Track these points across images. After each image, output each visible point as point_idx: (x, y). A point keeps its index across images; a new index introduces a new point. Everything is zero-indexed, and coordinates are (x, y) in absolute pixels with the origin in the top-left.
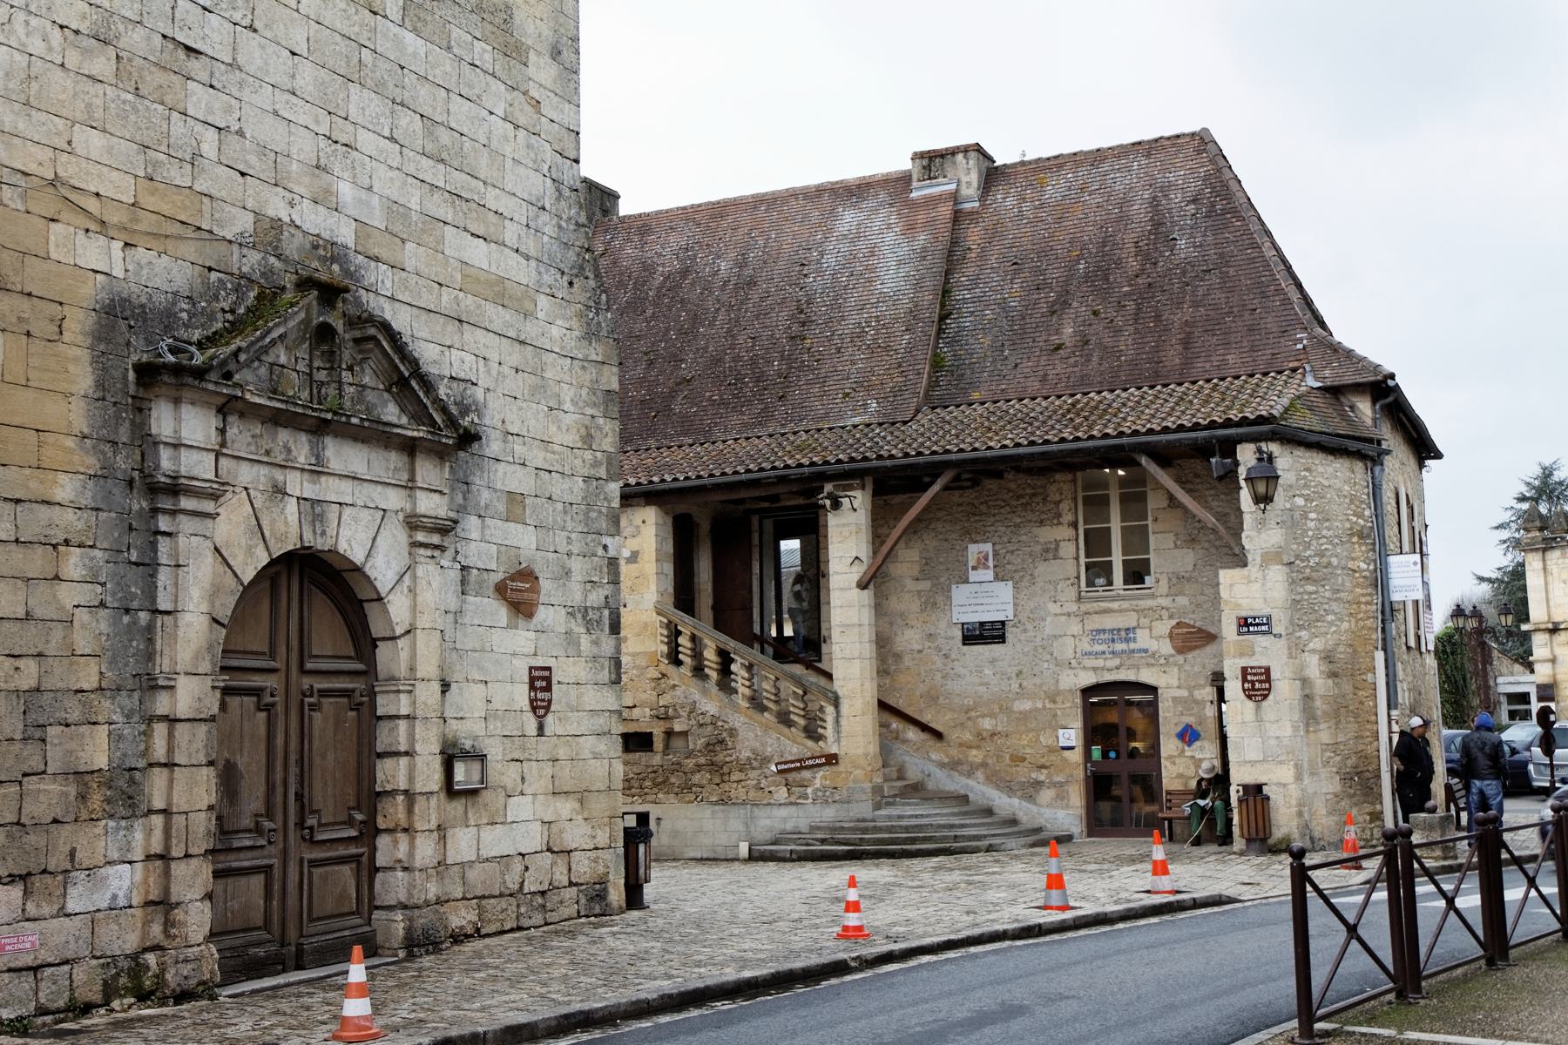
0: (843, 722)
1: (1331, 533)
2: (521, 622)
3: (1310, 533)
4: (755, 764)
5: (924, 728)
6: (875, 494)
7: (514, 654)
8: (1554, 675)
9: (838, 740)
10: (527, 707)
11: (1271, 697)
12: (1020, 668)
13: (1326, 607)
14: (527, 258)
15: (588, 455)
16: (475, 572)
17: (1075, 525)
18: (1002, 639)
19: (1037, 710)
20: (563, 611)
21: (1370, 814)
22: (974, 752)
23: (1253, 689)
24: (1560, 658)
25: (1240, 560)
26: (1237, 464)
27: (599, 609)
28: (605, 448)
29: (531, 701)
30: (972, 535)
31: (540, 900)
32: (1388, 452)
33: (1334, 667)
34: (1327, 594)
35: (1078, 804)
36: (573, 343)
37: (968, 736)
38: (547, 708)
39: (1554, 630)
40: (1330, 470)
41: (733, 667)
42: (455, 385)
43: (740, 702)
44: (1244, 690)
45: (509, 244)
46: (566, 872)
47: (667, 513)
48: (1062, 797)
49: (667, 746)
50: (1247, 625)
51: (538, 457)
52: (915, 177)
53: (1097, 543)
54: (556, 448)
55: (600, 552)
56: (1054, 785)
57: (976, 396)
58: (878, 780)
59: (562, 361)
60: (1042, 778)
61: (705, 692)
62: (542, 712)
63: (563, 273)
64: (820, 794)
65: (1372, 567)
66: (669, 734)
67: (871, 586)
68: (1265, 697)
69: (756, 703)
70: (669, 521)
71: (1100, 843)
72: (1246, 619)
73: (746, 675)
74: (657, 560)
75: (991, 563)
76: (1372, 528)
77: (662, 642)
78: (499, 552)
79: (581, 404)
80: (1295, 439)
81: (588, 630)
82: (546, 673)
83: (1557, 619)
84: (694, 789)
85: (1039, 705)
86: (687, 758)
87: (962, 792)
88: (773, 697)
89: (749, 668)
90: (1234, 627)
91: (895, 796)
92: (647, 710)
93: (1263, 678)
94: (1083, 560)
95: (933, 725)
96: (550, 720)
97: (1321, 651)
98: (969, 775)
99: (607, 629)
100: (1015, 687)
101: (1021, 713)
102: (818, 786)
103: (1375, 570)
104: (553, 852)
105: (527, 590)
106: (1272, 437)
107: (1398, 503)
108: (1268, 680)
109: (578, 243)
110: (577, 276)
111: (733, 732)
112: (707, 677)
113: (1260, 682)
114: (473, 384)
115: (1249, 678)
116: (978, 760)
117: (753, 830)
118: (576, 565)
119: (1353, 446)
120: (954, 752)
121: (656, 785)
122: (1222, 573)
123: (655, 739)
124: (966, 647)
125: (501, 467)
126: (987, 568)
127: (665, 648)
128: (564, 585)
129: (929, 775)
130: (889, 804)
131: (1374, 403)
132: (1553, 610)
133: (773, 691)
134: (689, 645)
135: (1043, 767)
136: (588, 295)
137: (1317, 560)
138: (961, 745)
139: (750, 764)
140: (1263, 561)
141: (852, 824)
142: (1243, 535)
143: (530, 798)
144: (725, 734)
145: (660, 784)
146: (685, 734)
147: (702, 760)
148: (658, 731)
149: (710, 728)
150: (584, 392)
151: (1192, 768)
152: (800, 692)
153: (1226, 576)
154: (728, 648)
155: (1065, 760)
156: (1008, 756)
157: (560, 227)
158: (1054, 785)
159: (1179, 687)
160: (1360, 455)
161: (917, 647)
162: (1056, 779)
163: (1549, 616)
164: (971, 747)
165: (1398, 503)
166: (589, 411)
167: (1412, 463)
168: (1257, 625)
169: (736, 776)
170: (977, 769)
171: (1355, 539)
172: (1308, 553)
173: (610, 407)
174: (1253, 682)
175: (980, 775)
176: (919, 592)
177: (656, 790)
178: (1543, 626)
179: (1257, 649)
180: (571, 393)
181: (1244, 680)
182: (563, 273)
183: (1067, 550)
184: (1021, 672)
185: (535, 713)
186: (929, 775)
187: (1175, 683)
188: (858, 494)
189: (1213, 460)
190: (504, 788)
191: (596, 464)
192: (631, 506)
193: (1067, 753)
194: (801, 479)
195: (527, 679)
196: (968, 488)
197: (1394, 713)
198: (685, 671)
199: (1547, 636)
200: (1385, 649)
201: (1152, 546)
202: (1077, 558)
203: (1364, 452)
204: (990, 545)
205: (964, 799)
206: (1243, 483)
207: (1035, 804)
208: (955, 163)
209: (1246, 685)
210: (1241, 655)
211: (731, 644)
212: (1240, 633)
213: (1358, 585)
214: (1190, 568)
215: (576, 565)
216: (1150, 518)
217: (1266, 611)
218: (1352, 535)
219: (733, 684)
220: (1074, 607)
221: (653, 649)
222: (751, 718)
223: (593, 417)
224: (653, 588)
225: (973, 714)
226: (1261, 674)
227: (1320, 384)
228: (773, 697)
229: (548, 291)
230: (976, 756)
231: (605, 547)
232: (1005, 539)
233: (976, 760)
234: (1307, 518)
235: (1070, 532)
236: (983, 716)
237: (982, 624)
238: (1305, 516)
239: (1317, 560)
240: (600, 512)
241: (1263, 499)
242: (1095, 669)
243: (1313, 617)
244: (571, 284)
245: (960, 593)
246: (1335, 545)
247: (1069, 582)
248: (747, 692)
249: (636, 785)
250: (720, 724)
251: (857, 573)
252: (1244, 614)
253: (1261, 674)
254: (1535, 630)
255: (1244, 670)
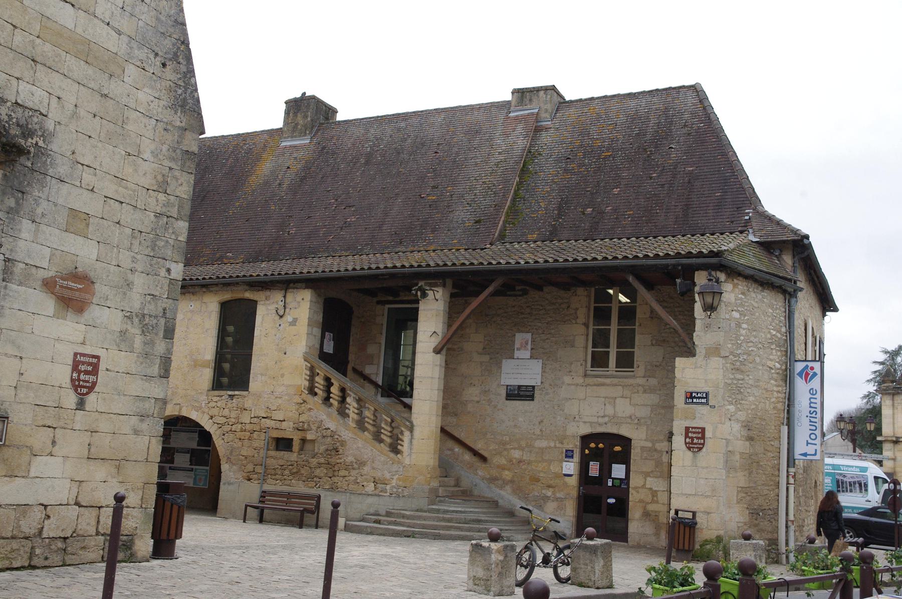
0: (415, 442)
1: (757, 340)
2: (70, 315)
3: (742, 338)
4: (356, 466)
5: (475, 453)
6: (452, 296)
7: (58, 340)
8: (894, 468)
9: (410, 455)
10: (69, 385)
11: (704, 450)
12: (542, 418)
13: (749, 390)
14: (119, 33)
15: (161, 197)
16: (22, 266)
17: (586, 325)
18: (531, 398)
19: (550, 447)
20: (121, 314)
21: (769, 540)
22: (507, 472)
23: (692, 443)
24: (899, 458)
25: (690, 352)
26: (694, 284)
27: (156, 317)
28: (179, 194)
29: (72, 380)
30: (521, 327)
31: (60, 544)
32: (801, 289)
33: (751, 433)
34: (751, 382)
35: (571, 514)
36: (160, 110)
37: (503, 461)
38: (91, 389)
39: (896, 442)
40: (760, 297)
41: (348, 400)
42: (20, 110)
43: (350, 423)
44: (686, 443)
45: (100, 17)
46: (94, 523)
47: (319, 295)
48: (561, 508)
49: (301, 449)
50: (692, 397)
51: (110, 188)
52: (513, 104)
53: (601, 339)
54: (129, 185)
55: (163, 272)
56: (557, 499)
57: (530, 237)
58: (435, 484)
59: (145, 120)
60: (549, 494)
61: (329, 415)
62: (85, 391)
63: (157, 54)
64: (395, 490)
65: (784, 367)
66: (304, 441)
67: (444, 352)
68: (700, 449)
69: (361, 425)
70: (321, 301)
71: (395, 540)
72: (691, 393)
73: (356, 406)
74: (308, 325)
75: (529, 347)
76: (786, 340)
77: (305, 379)
78: (52, 255)
79: (161, 157)
80: (734, 272)
81: (143, 331)
82: (94, 361)
83: (898, 436)
84: (315, 479)
85: (552, 444)
86: (313, 458)
87: (496, 499)
88: (371, 422)
89: (359, 401)
90: (683, 398)
91: (447, 496)
92: (291, 423)
93: (700, 435)
94: (590, 350)
95: (481, 452)
96: (91, 399)
97: (743, 421)
98: (501, 488)
99: (161, 334)
100: (538, 432)
101: (540, 448)
102: (394, 484)
103: (786, 370)
104: (80, 506)
105: (79, 290)
106: (722, 267)
107: (806, 330)
108: (703, 437)
109: (175, 36)
110: (170, 60)
111: (343, 443)
112: (331, 405)
113: (698, 438)
114: (41, 114)
115: (690, 435)
116: (508, 478)
117: (349, 510)
118: (139, 281)
119: (778, 282)
120: (494, 472)
121: (292, 474)
122: (677, 359)
123: (294, 443)
124: (508, 402)
125: (65, 188)
126: (527, 349)
127: (307, 383)
128: (125, 294)
129: (476, 485)
130: (440, 501)
131: (794, 257)
132: (896, 430)
133: (372, 417)
134: (322, 382)
135: (549, 486)
136: (179, 76)
137: (745, 357)
138: (498, 467)
139: (352, 466)
140: (706, 353)
141: (412, 513)
142: (694, 334)
143: (60, 460)
144: (338, 444)
145: (294, 473)
146: (313, 441)
147: (322, 460)
148: (296, 438)
149: (329, 439)
150: (165, 148)
151: (650, 496)
152: (389, 420)
153: (680, 362)
154: (346, 386)
155: (565, 484)
156: (528, 477)
157: (158, 19)
158: (557, 499)
159: (645, 440)
160: (784, 292)
161: (477, 399)
162: (558, 495)
163: (894, 432)
164: (504, 469)
165: (806, 330)
166: (167, 163)
167: (817, 311)
168: (699, 398)
169: (343, 473)
170: (507, 484)
171: (773, 347)
172: (739, 351)
173: (188, 164)
174: (692, 438)
175: (508, 488)
176: (481, 363)
177: (291, 477)
178: (890, 439)
179: (698, 415)
180: (153, 147)
181: (687, 436)
182: (157, 54)
183: (580, 341)
184: (542, 421)
185: (76, 391)
186: (476, 485)
187: (643, 436)
188: (440, 290)
189: (678, 281)
190: (30, 448)
191: (167, 204)
192: (297, 288)
193: (567, 479)
194: (404, 276)
195: (71, 363)
196: (520, 296)
197: (792, 470)
198: (318, 400)
199: (892, 445)
200: (788, 425)
201: (637, 343)
202: (586, 348)
203: (788, 293)
204: (530, 334)
205: (495, 504)
206: (697, 297)
207: (543, 511)
208: (538, 96)
209: (688, 440)
210: (686, 418)
211: (348, 384)
212: (686, 403)
213: (772, 378)
214: (661, 359)
215: (139, 281)
216: (637, 324)
217: (706, 389)
218: (772, 343)
219: (347, 411)
220: (580, 380)
221: (300, 384)
222: (356, 434)
223: (170, 169)
224: (304, 343)
225: (508, 447)
226: (699, 433)
227: (758, 240)
228: (371, 422)
229: (139, 63)
230: (507, 474)
231: (169, 270)
232: (540, 332)
233: (507, 478)
234: (740, 327)
235: (582, 329)
236: (515, 449)
237: (519, 387)
238: (739, 325)
239: (745, 357)
240: (167, 242)
241: (710, 308)
242: (591, 423)
243: (739, 397)
244: (164, 65)
245: (508, 365)
246: (759, 349)
247: (579, 364)
248: (356, 417)
249: (279, 473)
250: (336, 437)
251: (434, 342)
252: (691, 390)
253: (699, 433)
254: (885, 441)
255: (687, 429)
